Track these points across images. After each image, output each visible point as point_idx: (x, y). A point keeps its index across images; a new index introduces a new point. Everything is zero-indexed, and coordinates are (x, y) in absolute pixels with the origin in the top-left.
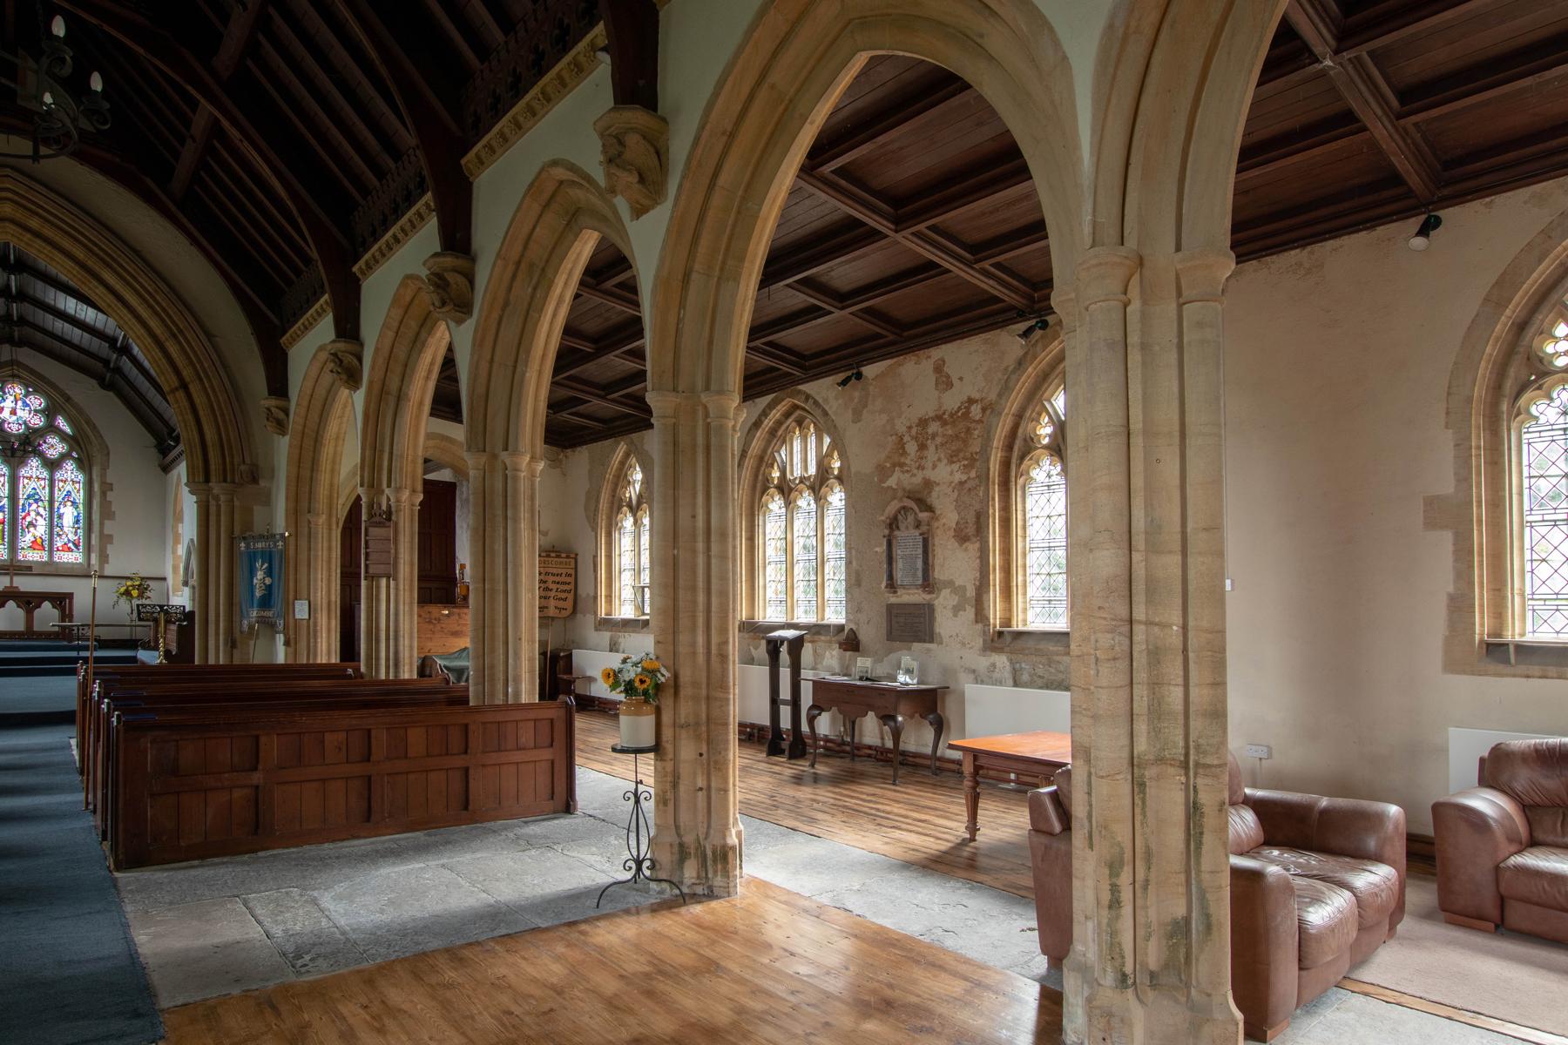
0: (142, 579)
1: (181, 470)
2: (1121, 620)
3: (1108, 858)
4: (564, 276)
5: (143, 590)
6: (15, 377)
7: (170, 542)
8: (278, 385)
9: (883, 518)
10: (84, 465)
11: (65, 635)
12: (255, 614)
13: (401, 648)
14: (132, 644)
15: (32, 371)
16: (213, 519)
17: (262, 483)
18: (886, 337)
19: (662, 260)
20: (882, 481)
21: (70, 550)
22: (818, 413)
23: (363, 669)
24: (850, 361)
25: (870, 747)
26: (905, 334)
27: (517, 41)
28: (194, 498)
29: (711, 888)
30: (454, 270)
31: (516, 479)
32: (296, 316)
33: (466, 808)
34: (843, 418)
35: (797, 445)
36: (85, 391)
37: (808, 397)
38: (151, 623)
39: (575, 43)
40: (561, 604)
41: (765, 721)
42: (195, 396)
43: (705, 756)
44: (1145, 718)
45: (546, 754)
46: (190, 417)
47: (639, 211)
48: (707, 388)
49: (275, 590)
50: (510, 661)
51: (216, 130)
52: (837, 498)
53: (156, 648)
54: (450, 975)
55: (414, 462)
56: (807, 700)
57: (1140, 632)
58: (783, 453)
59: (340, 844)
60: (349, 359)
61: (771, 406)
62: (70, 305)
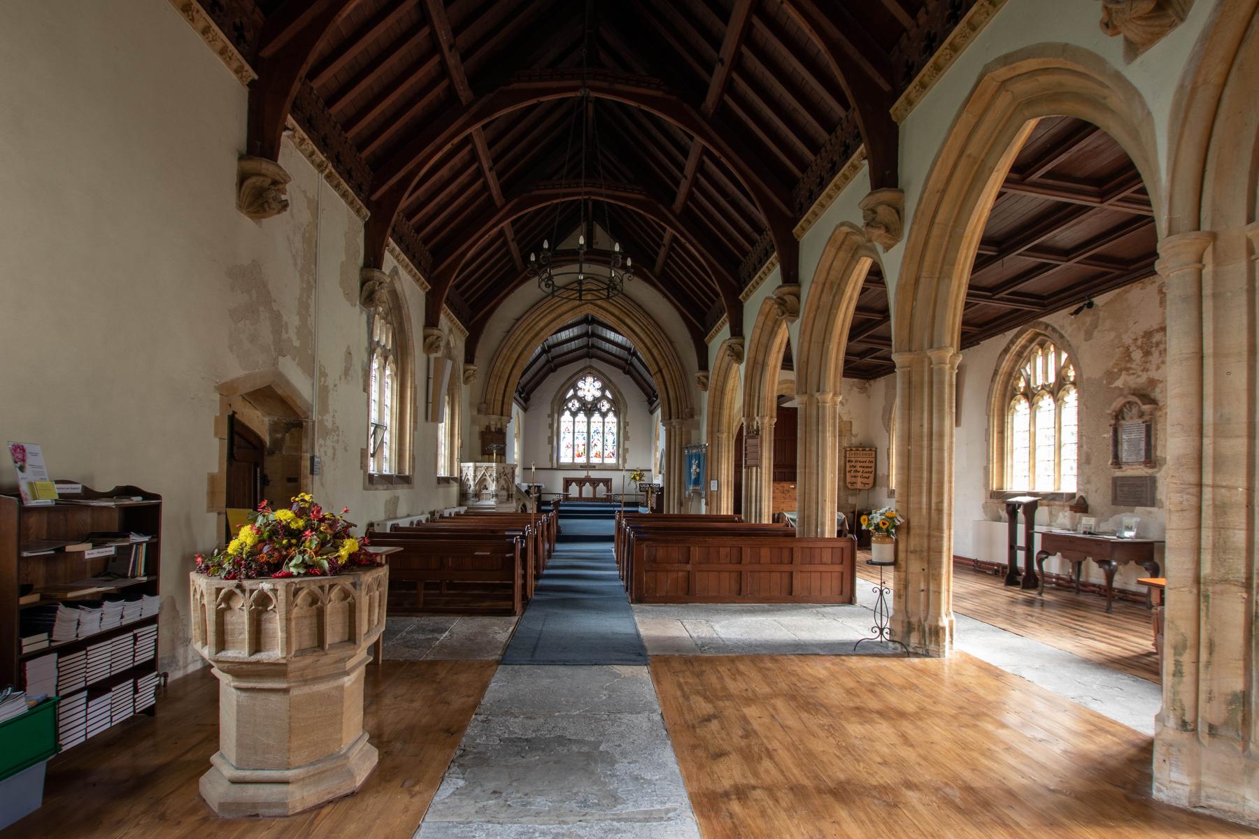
0: (641, 470)
1: (659, 412)
2: (1190, 484)
3: (1173, 642)
4: (852, 285)
5: (641, 476)
6: (590, 374)
7: (653, 451)
8: (704, 366)
9: (1109, 412)
10: (617, 414)
11: (608, 499)
12: (691, 488)
13: (763, 507)
14: (636, 504)
15: (599, 372)
16: (673, 438)
17: (696, 418)
18: (1112, 273)
19: (901, 275)
20: (1110, 383)
21: (611, 457)
22: (1056, 336)
23: (743, 518)
24: (1082, 295)
25: (1094, 585)
26: (1132, 267)
27: (821, 159)
28: (664, 428)
29: (927, 651)
30: (790, 294)
31: (824, 408)
32: (712, 325)
33: (791, 594)
34: (1077, 340)
35: (1039, 361)
36: (617, 376)
37: (1047, 326)
38: (645, 493)
39: (853, 153)
40: (865, 481)
41: (1005, 561)
42: (665, 375)
43: (926, 570)
44: (1210, 551)
45: (838, 568)
46: (663, 386)
47: (887, 248)
48: (931, 346)
49: (701, 475)
50: (819, 514)
51: (675, 239)
52: (1071, 398)
53: (647, 506)
54: (769, 665)
55: (772, 401)
56: (1037, 547)
57: (1208, 493)
58: (1028, 368)
59: (725, 605)
60: (737, 347)
61: (1017, 336)
62: (611, 335)
